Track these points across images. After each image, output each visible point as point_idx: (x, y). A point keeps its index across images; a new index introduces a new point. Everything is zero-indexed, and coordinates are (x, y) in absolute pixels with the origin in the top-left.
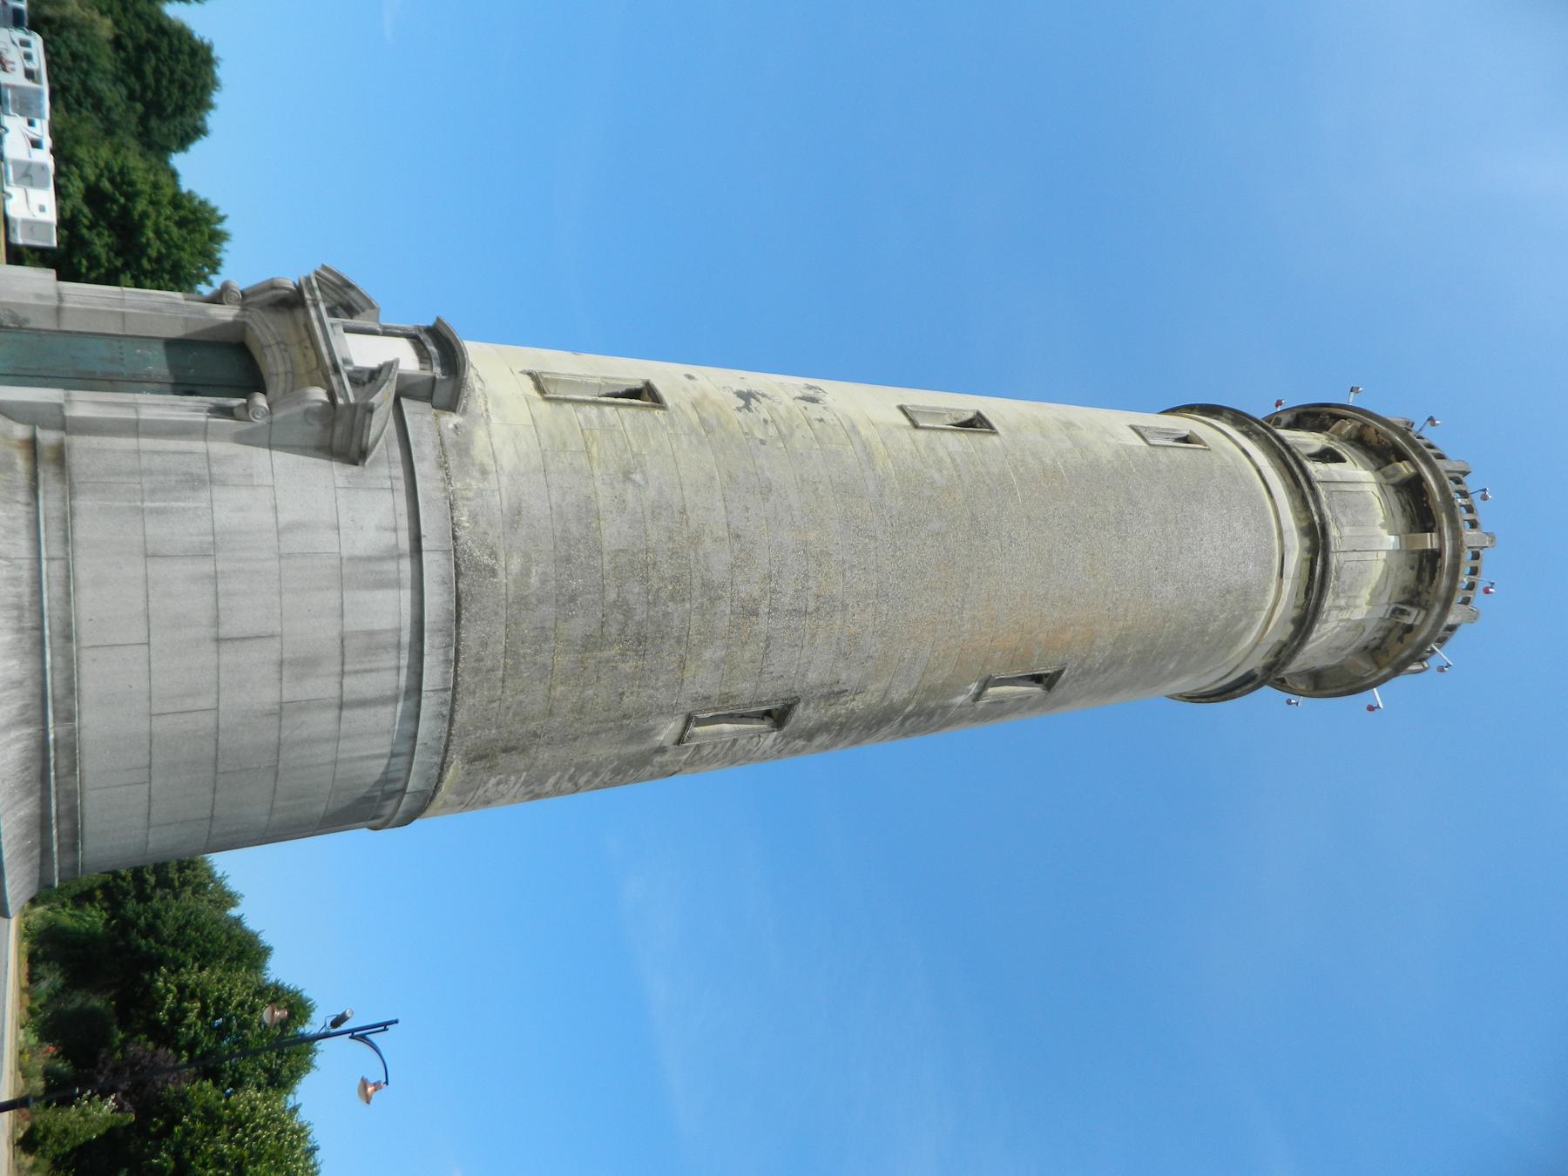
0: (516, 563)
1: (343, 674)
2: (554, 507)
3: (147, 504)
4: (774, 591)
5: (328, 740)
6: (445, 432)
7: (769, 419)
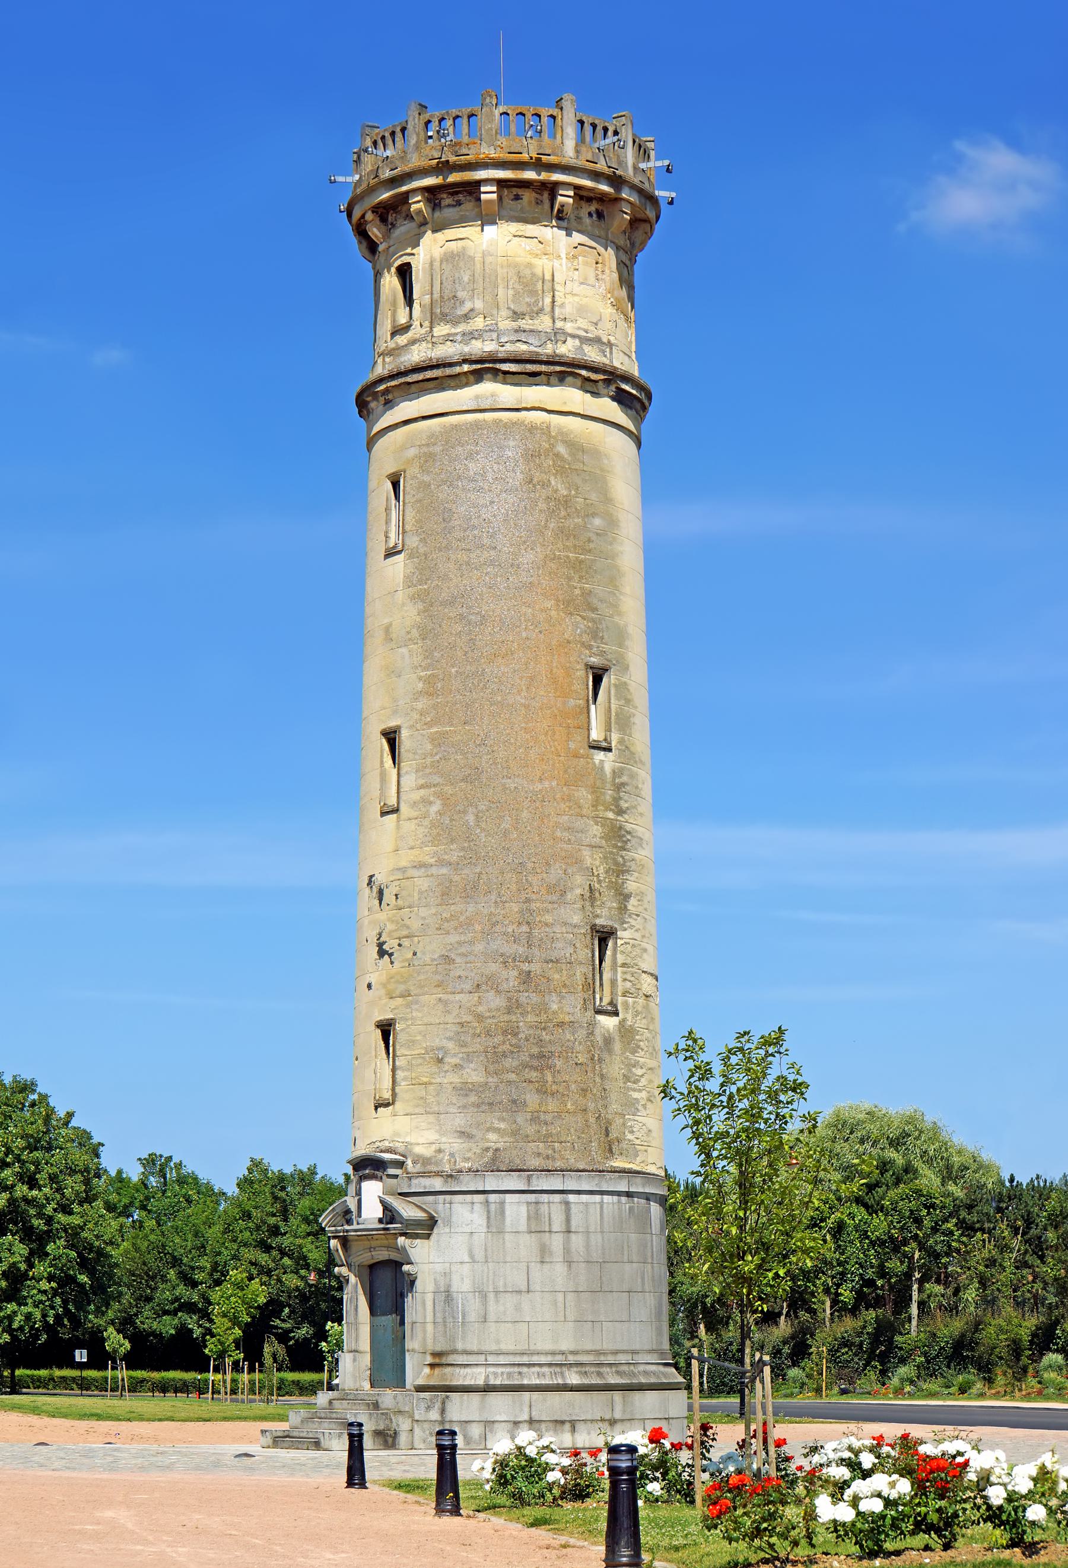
0: (493, 1136)
4: (514, 960)
5: (588, 1238)
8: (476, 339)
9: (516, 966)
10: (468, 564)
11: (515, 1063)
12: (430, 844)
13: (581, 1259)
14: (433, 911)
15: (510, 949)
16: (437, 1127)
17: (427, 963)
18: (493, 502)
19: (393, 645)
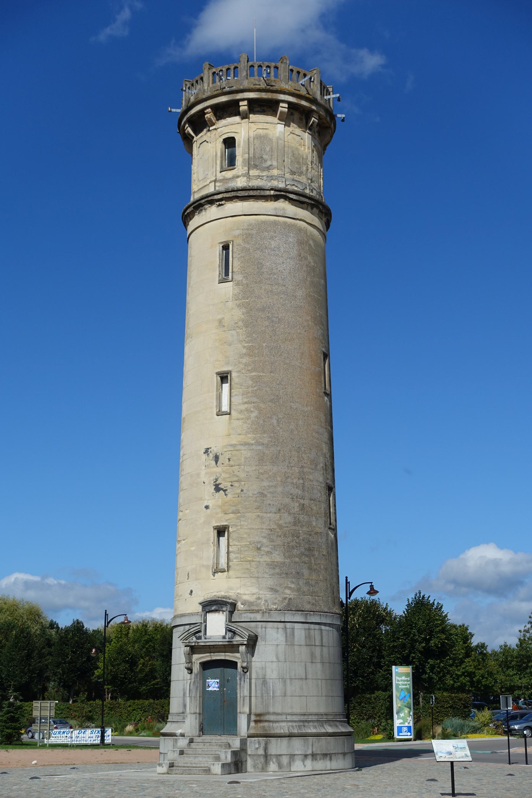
0: (288, 591)
1: (315, 645)
2: (270, 577)
3: (271, 695)
4: (297, 497)
6: (245, 609)
7: (230, 483)
8: (274, 180)
9: (298, 500)
10: (271, 291)
11: (298, 552)
12: (251, 433)
13: (327, 662)
14: (254, 468)
15: (295, 491)
16: (257, 585)
17: (250, 496)
18: (284, 263)
19: (225, 329)
